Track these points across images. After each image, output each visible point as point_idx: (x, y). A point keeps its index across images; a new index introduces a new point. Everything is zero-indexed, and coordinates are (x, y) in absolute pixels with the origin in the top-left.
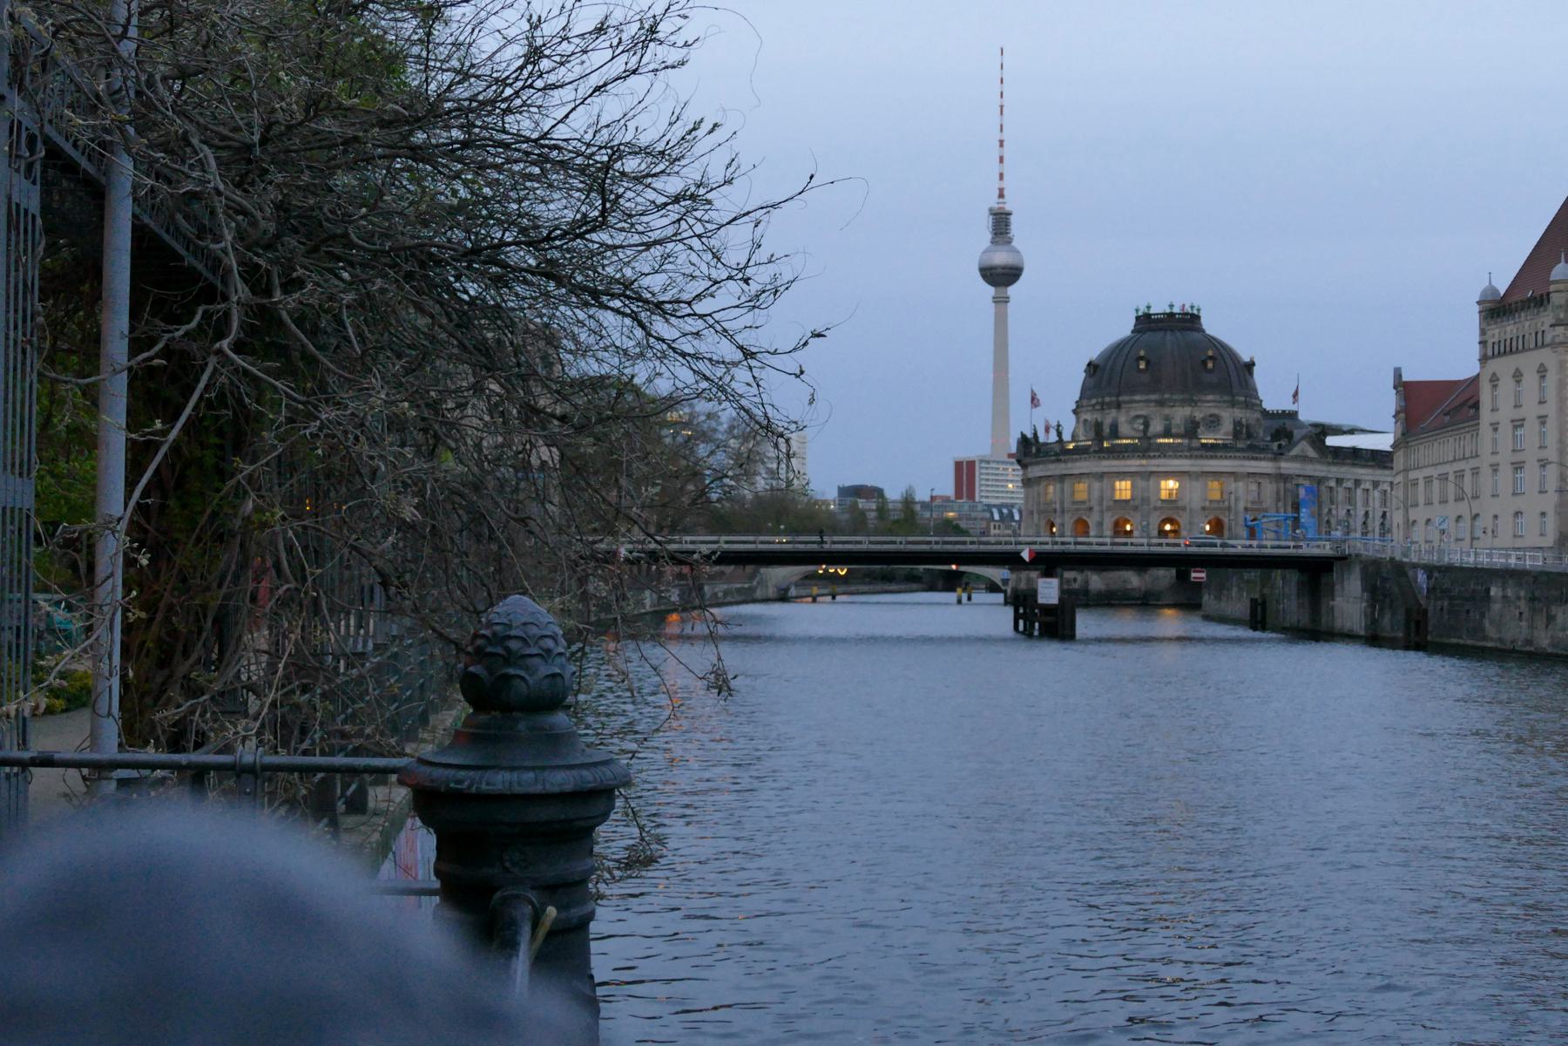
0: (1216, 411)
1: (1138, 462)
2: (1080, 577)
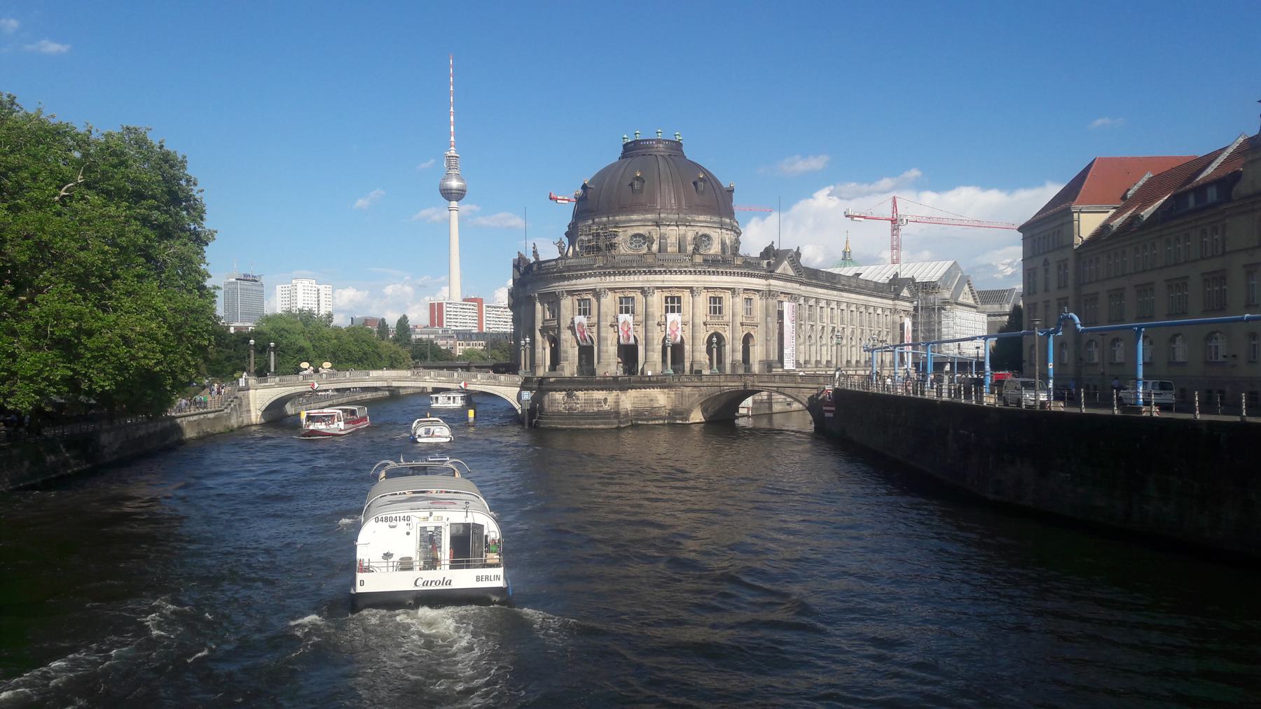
0: (707, 231)
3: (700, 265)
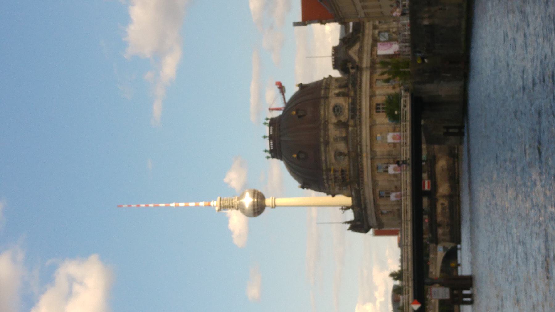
0: (331, 109)
1: (365, 159)
2: (441, 201)
3: (355, 121)
